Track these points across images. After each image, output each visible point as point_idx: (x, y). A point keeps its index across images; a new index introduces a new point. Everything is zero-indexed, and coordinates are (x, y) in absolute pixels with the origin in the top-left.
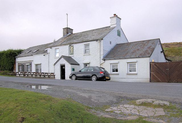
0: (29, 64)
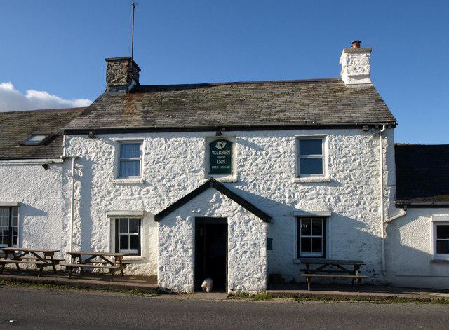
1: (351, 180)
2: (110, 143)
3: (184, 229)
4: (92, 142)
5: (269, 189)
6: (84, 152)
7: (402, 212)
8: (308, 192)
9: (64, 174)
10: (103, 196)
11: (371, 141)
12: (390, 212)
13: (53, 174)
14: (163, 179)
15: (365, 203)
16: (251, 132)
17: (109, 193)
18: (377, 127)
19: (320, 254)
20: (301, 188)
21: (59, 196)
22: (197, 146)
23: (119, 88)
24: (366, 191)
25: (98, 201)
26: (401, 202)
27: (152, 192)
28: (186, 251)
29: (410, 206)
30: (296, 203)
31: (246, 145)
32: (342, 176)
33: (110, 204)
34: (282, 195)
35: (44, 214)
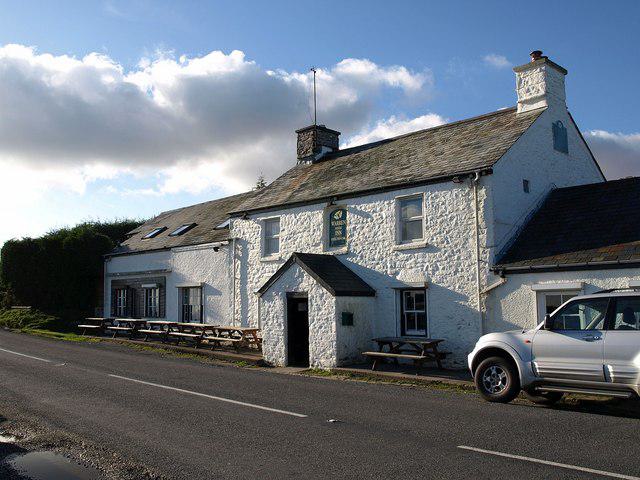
0: (154, 285)
1: (448, 243)
3: (278, 305)
4: (246, 223)
5: (374, 260)
8: (407, 260)
11: (468, 194)
12: (489, 281)
13: (222, 255)
15: (462, 270)
18: (471, 176)
19: (423, 333)
20: (401, 256)
22: (317, 217)
23: (306, 159)
24: (463, 254)
28: (280, 325)
30: (397, 273)
31: (355, 213)
32: (439, 240)
34: (385, 266)
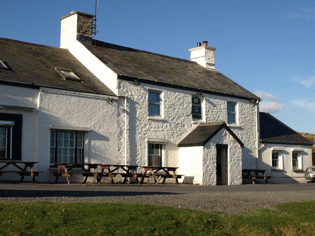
2: (145, 90)
6: (130, 94)
7: (263, 145)
9: (118, 109)
10: (142, 128)
14: (174, 118)
16: (216, 96)
17: (146, 125)
21: (116, 126)
25: (140, 131)
26: (264, 140)
27: (168, 127)
28: (214, 163)
29: (267, 143)
33: (147, 133)
35: (107, 139)
